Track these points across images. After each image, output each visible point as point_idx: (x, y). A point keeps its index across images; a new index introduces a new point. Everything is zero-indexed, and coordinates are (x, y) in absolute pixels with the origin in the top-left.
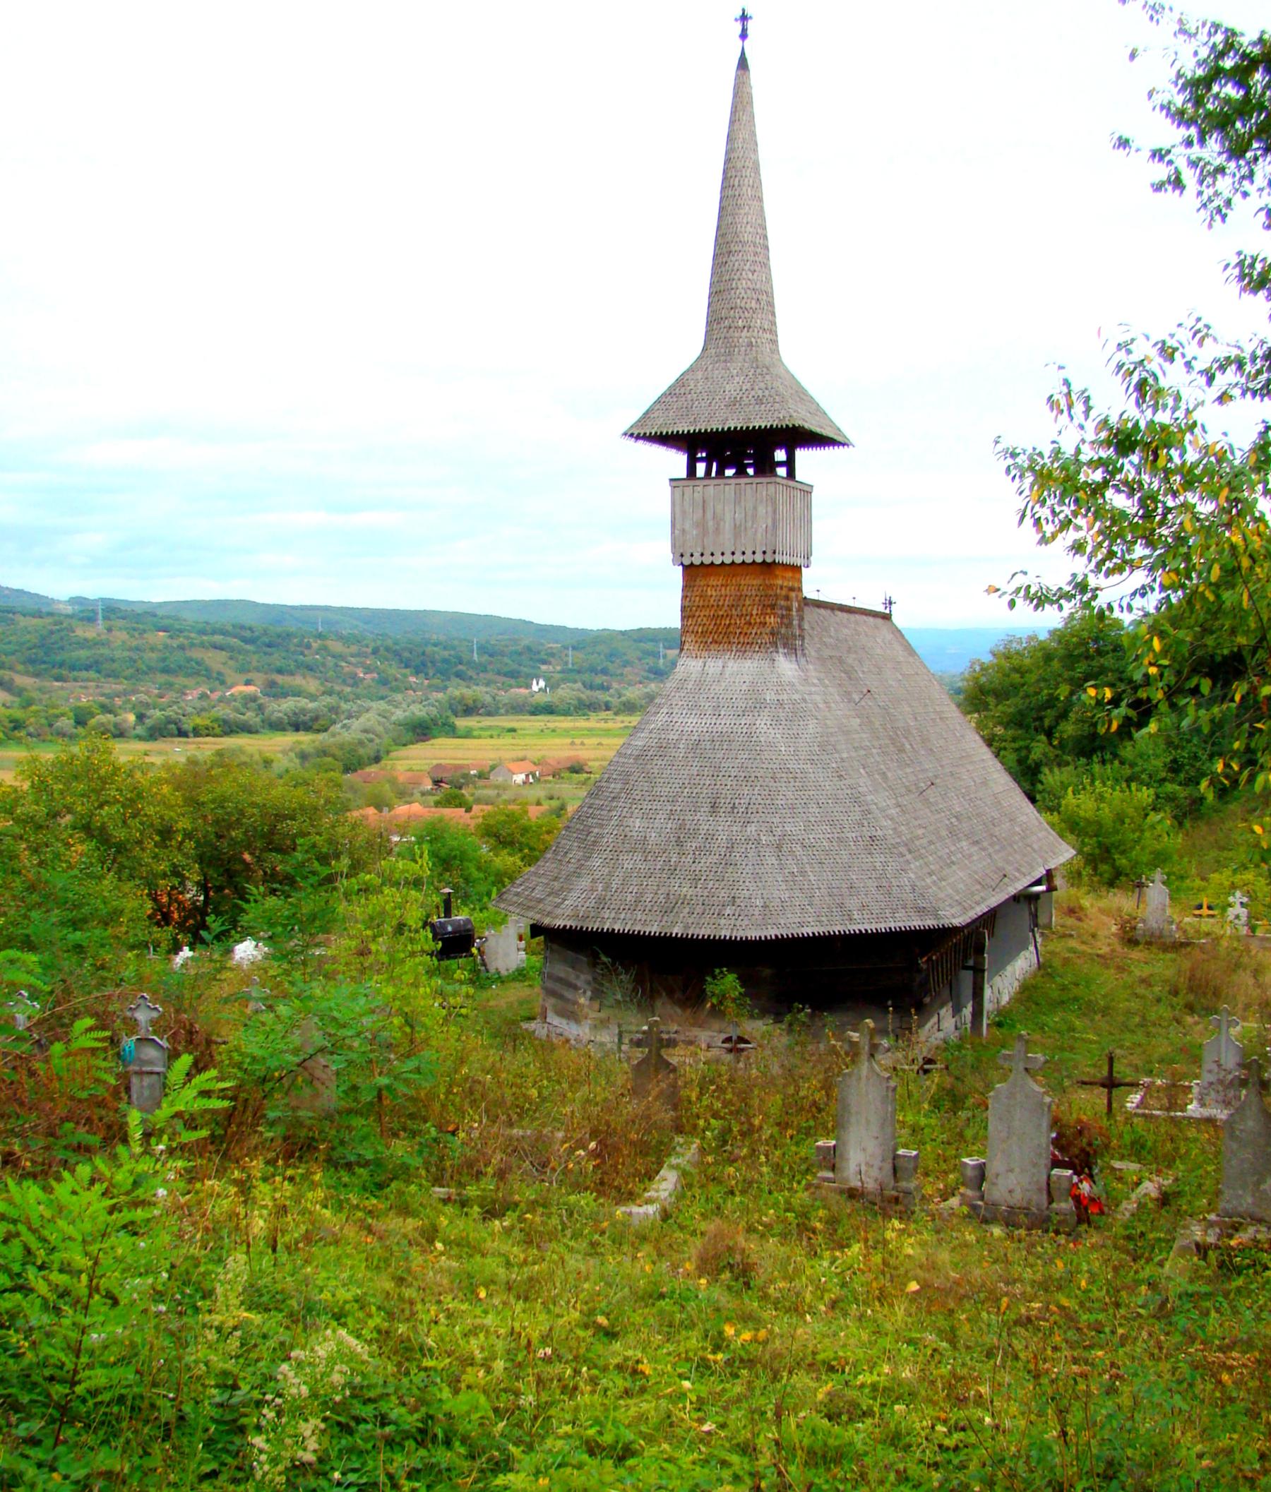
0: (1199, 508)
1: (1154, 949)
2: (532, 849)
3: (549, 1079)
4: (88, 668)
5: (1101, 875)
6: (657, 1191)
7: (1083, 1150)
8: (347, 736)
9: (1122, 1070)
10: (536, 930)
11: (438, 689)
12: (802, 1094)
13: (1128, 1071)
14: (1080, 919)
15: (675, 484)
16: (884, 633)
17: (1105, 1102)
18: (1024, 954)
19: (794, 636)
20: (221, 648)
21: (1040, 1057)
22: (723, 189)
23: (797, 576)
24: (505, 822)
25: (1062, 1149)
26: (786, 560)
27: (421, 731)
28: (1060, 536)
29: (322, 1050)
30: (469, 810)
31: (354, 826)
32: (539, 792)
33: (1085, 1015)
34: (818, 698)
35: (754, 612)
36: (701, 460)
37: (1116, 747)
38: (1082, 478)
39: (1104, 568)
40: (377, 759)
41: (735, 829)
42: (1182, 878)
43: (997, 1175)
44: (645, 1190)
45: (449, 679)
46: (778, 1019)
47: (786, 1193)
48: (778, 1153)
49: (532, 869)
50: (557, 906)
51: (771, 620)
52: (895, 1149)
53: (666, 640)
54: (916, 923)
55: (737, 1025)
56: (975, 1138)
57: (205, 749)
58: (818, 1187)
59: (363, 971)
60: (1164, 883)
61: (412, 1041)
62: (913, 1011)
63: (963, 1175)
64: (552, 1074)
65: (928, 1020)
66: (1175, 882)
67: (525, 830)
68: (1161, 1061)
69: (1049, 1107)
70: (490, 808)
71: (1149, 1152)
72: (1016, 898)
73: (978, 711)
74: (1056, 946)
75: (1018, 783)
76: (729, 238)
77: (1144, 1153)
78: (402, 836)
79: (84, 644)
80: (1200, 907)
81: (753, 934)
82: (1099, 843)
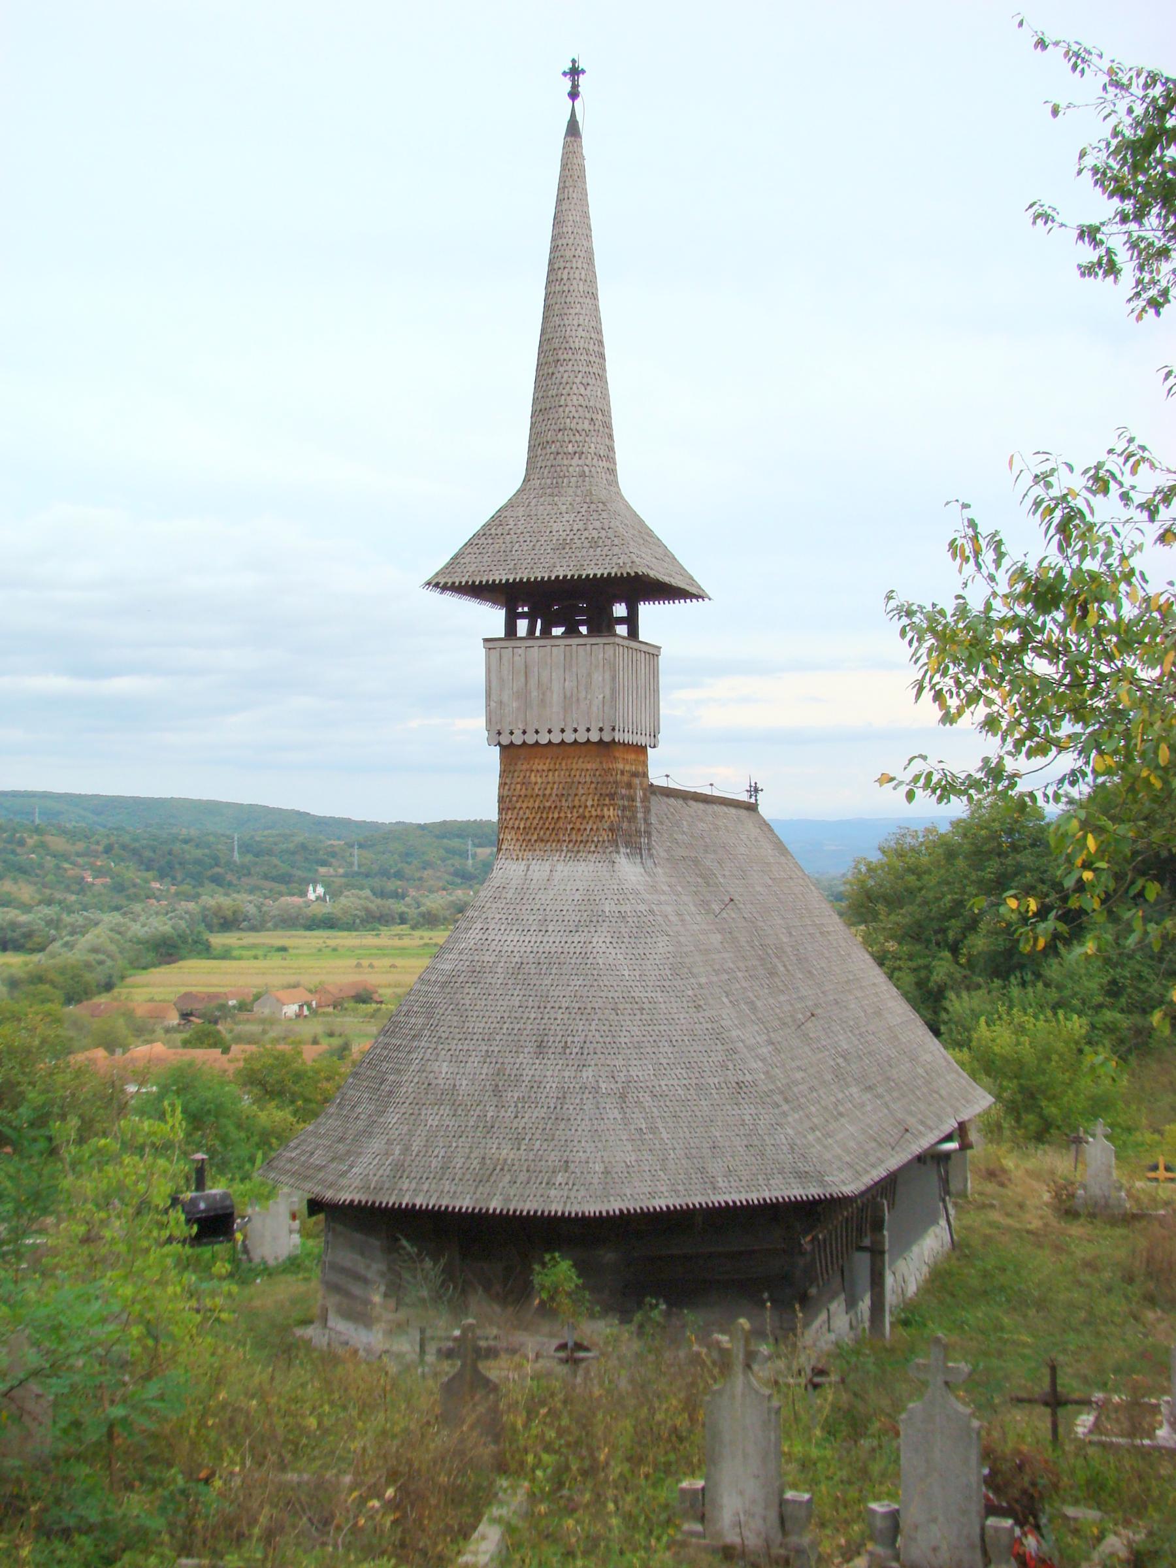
0: (1141, 674)
1: (1097, 1222)
2: (307, 1100)
3: (332, 1403)
5: (1026, 1127)
6: (476, 1553)
7: (1025, 1492)
8: (75, 956)
9: (1069, 1384)
10: (315, 1206)
12: (659, 1417)
13: (1075, 1383)
14: (1002, 1185)
15: (490, 645)
16: (750, 828)
17: (1049, 1425)
18: (933, 1230)
19: (638, 831)
21: (965, 1367)
22: (549, 282)
23: (642, 758)
24: (272, 1066)
25: (997, 1490)
26: (627, 738)
28: (968, 712)
29: (36, 1373)
30: (226, 1050)
31: (79, 1073)
32: (315, 1027)
33: (1015, 1309)
34: (669, 909)
35: (589, 803)
36: (523, 616)
37: (1039, 965)
38: (994, 640)
39: (1024, 749)
40: (108, 987)
41: (567, 1074)
42: (1129, 1130)
43: (916, 1527)
44: (459, 1553)
45: (201, 885)
46: (626, 1317)
47: (642, 1553)
48: (629, 1498)
49: (310, 1128)
50: (344, 1174)
51: (610, 812)
52: (781, 1492)
55: (574, 1327)
56: (883, 1474)
58: (684, 1544)
59: (93, 1263)
60: (1107, 1137)
61: (154, 1357)
62: (797, 1306)
63: (871, 1525)
64: (336, 1396)
65: (816, 1316)
66: (1120, 1134)
67: (299, 1076)
68: (1117, 1370)
69: (978, 1434)
70: (254, 1048)
71: (1111, 1495)
72: (920, 1159)
73: (865, 922)
74: (973, 1219)
75: (918, 1011)
76: (556, 343)
77: (1103, 1495)
78: (141, 1085)
80: (1155, 1168)
81: (592, 1208)
82: (1021, 1085)
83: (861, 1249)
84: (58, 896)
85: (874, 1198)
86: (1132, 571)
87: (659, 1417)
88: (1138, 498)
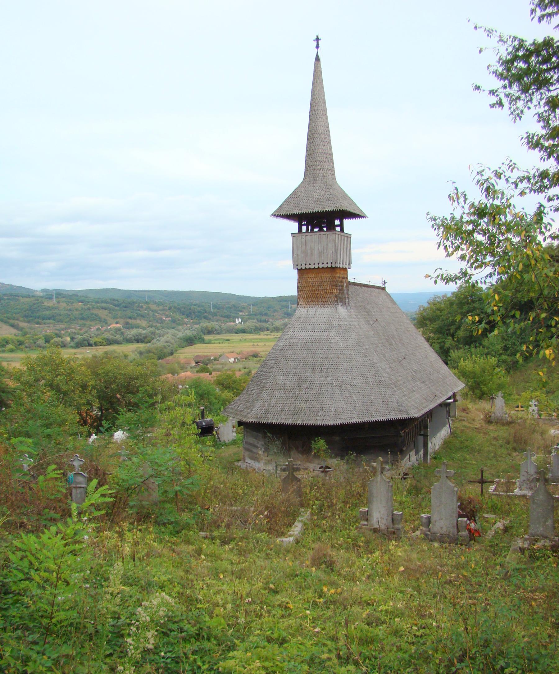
0: (513, 240)
1: (499, 425)
2: (237, 390)
3: (247, 485)
4: (50, 319)
6: (293, 531)
7: (471, 510)
8: (159, 344)
10: (240, 423)
11: (196, 324)
12: (353, 489)
13: (489, 476)
14: (467, 413)
19: (345, 298)
20: (105, 309)
22: (310, 111)
24: (226, 378)
25: (462, 509)
26: (341, 266)
27: (190, 341)
28: (455, 253)
29: (152, 476)
30: (211, 374)
31: (163, 382)
32: (240, 366)
33: (470, 453)
34: (356, 323)
35: (328, 288)
36: (304, 225)
38: (464, 228)
39: (474, 266)
40: (172, 354)
42: (510, 395)
45: (201, 319)
46: (342, 458)
48: (343, 514)
49: (238, 398)
50: (249, 413)
51: (335, 291)
52: (393, 511)
53: (291, 301)
54: (399, 416)
56: (426, 506)
57: (100, 351)
58: (361, 528)
59: (168, 442)
60: (502, 397)
61: (189, 471)
62: (399, 453)
63: (421, 521)
66: (507, 397)
67: (234, 382)
69: (457, 492)
70: (219, 373)
72: (440, 405)
73: (423, 327)
74: (458, 425)
75: (440, 357)
76: (313, 132)
78: (183, 386)
79: (48, 308)
80: (518, 407)
81: (331, 423)
82: (475, 381)
83: (421, 435)
84: (154, 324)
85: (425, 418)
86: (510, 204)
87: (353, 489)
88: (511, 180)
